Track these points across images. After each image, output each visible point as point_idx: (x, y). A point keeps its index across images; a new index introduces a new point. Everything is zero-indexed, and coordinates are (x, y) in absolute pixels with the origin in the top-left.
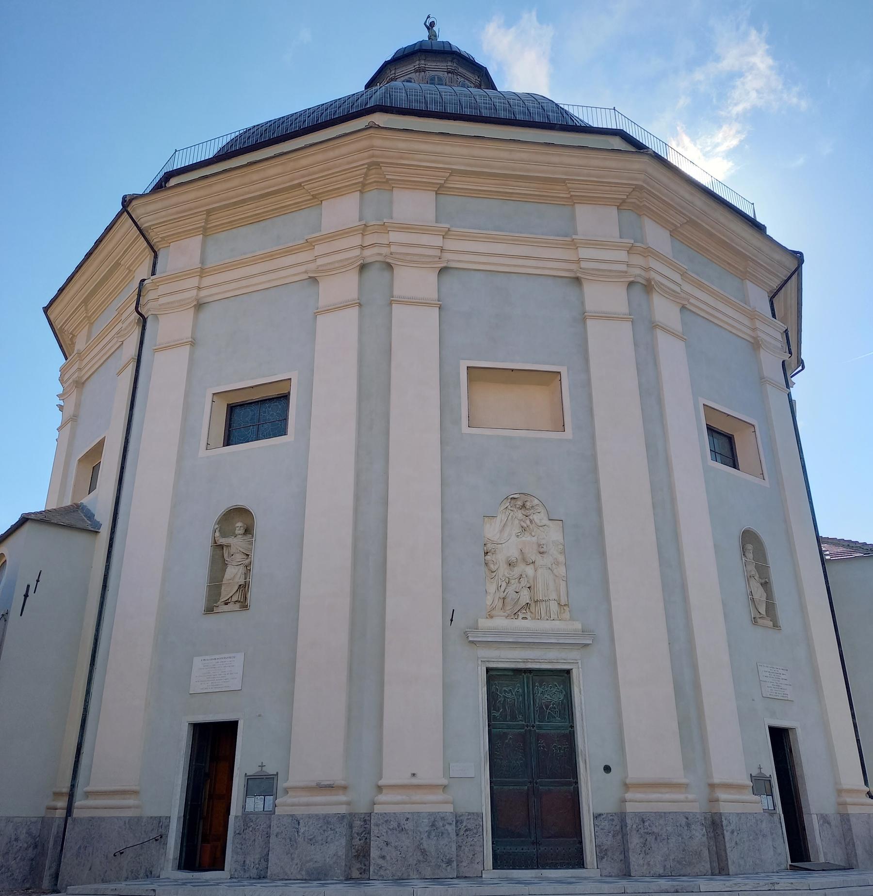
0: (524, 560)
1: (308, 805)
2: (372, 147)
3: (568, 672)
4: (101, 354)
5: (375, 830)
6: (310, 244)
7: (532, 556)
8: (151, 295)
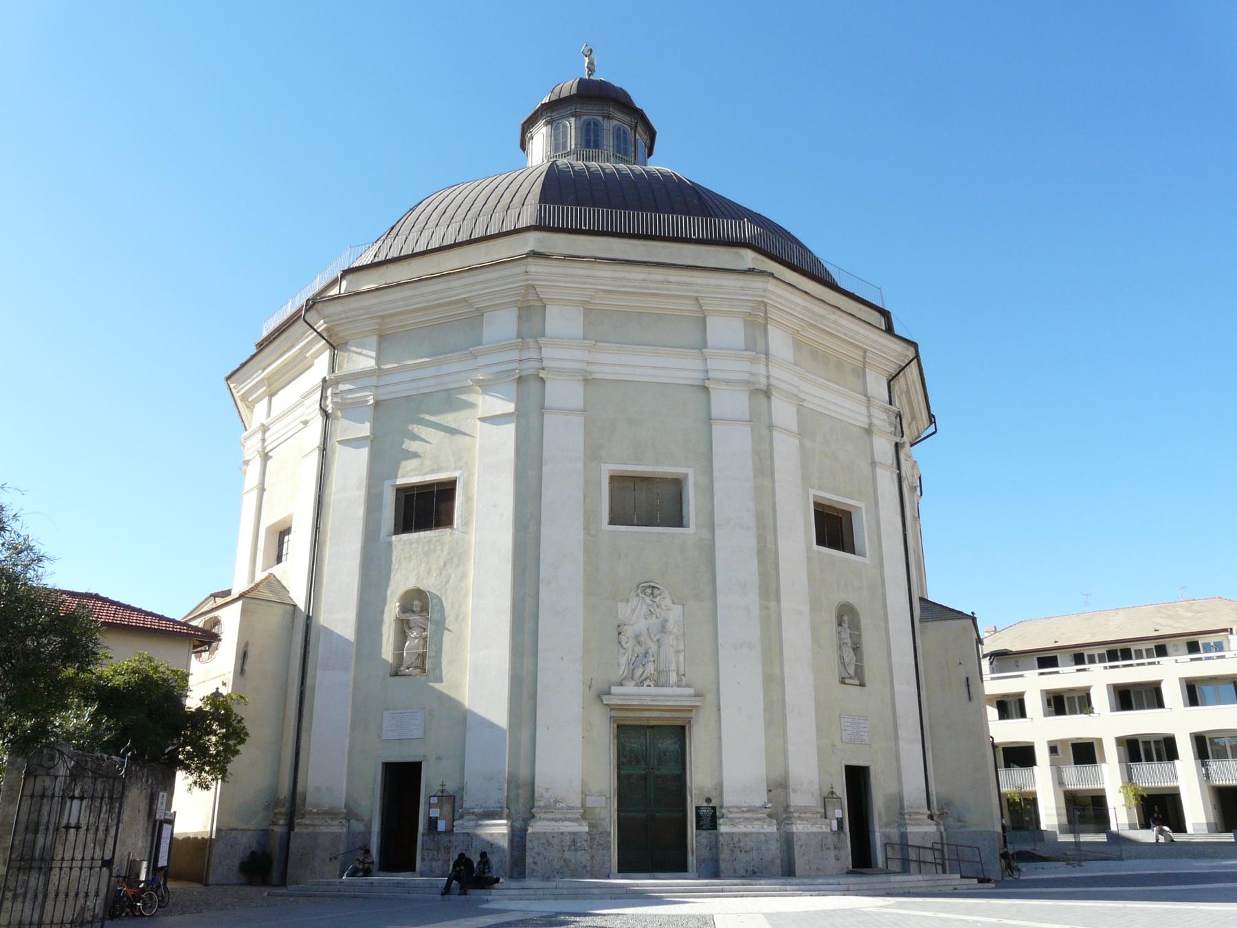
5: (529, 845)
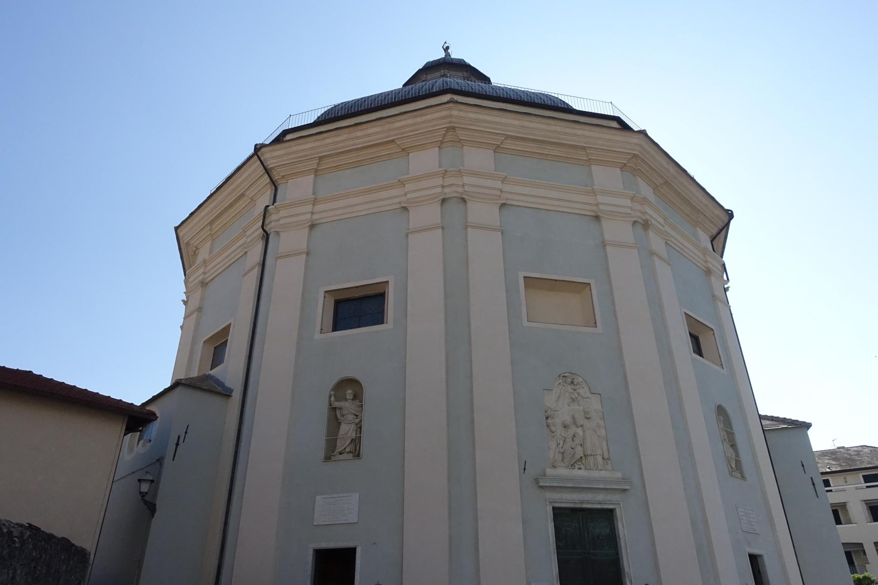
0: (575, 423)
2: (451, 116)
3: (611, 511)
6: (402, 183)
7: (581, 420)
8: (274, 217)
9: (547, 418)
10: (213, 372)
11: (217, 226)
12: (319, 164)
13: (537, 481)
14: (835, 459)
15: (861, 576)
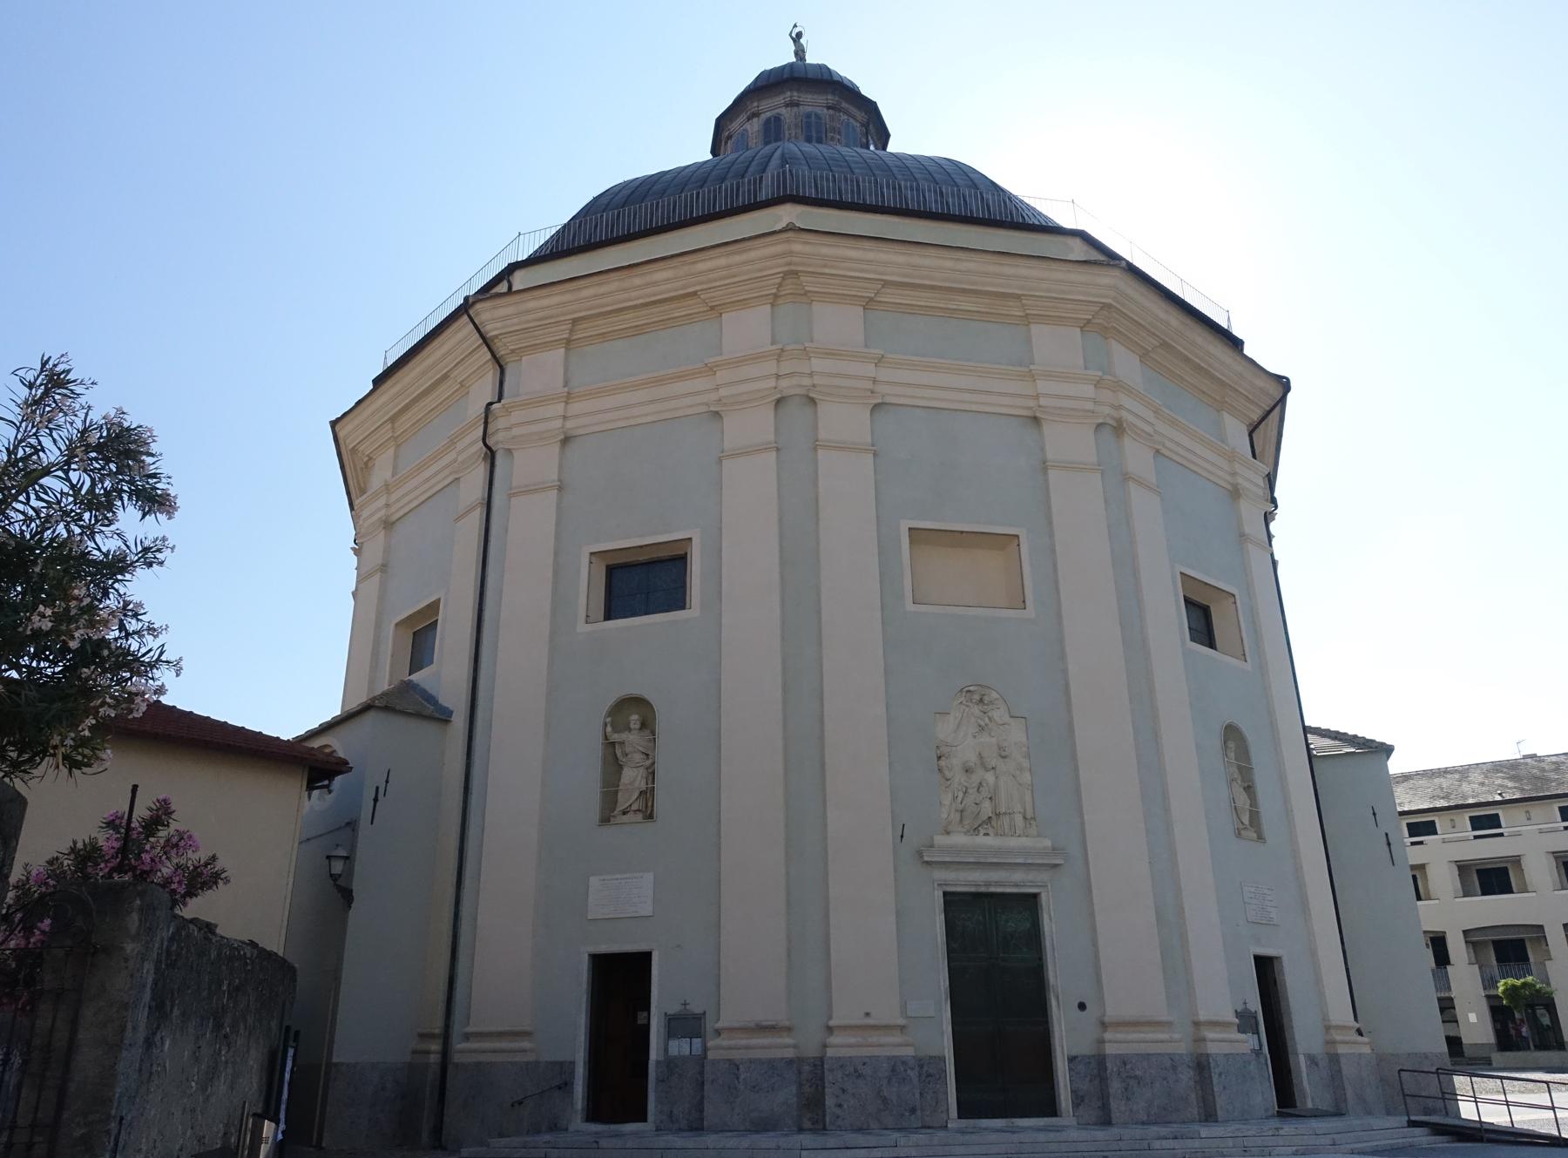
1: (747, 1048)
2: (791, 253)
3: (1034, 897)
4: (422, 489)
5: (829, 1077)
6: (711, 370)
9: (939, 758)
10: (415, 677)
11: (404, 422)
12: (571, 331)
13: (920, 854)
14: (1512, 778)
15: (1518, 983)
